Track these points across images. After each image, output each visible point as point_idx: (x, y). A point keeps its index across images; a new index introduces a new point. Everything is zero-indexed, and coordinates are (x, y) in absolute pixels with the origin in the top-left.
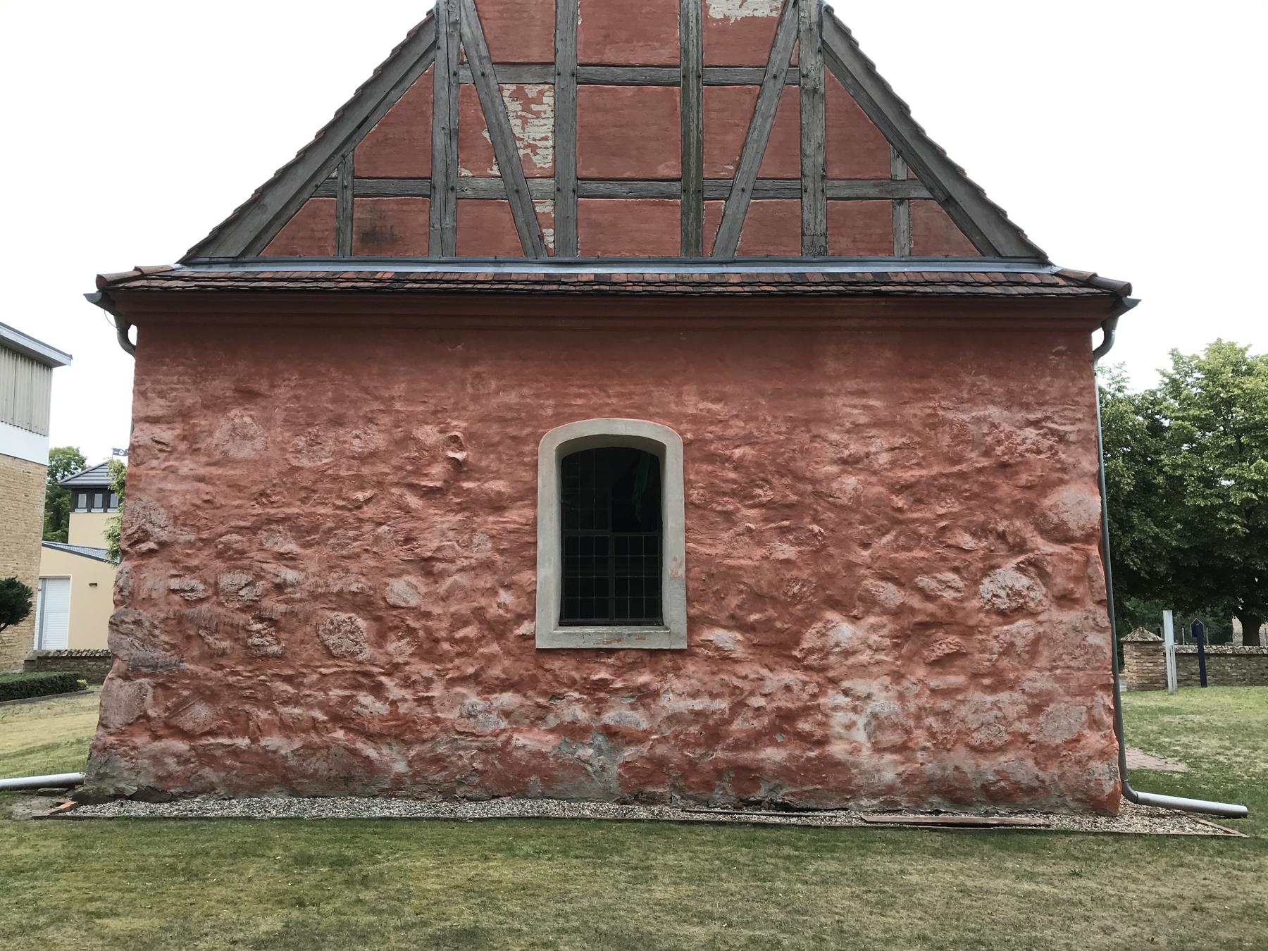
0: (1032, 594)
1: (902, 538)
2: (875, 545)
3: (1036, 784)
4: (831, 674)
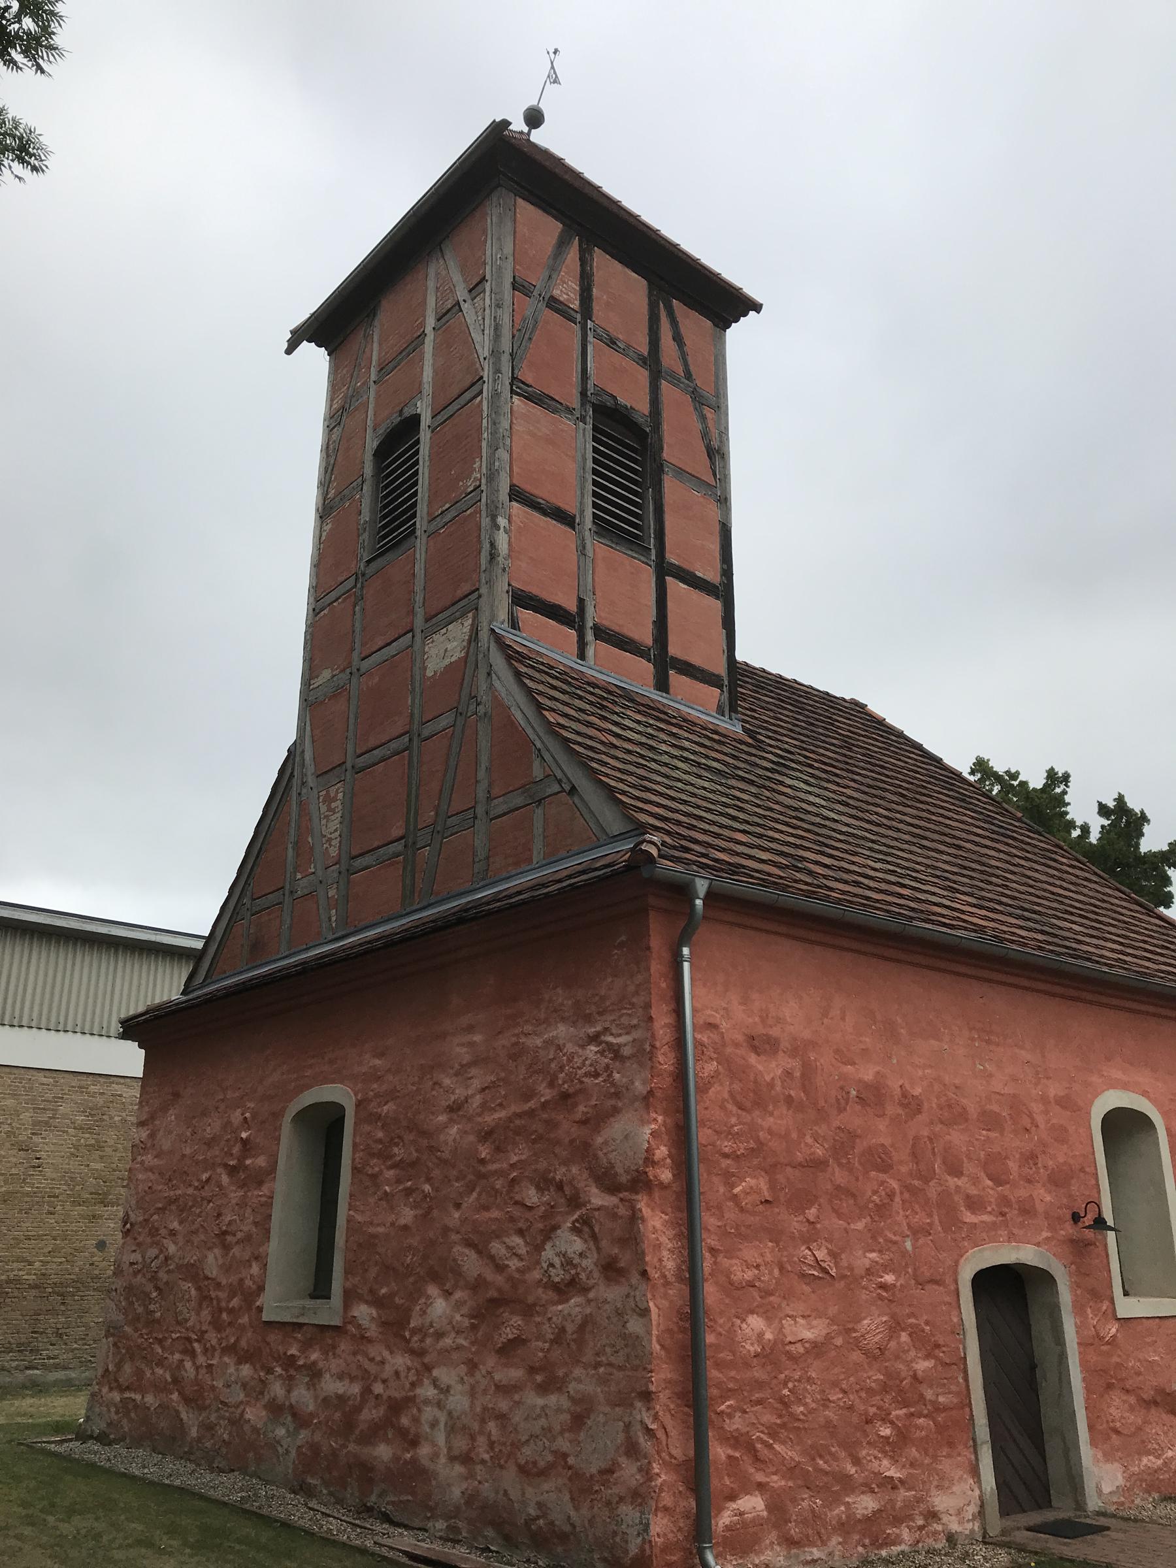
0: (584, 1263)
1: (484, 1195)
2: (465, 1205)
3: (567, 1528)
4: (426, 1360)
